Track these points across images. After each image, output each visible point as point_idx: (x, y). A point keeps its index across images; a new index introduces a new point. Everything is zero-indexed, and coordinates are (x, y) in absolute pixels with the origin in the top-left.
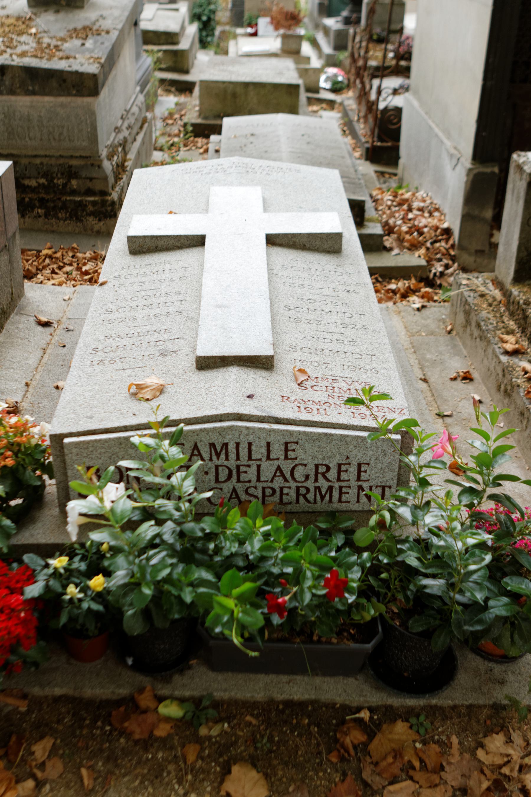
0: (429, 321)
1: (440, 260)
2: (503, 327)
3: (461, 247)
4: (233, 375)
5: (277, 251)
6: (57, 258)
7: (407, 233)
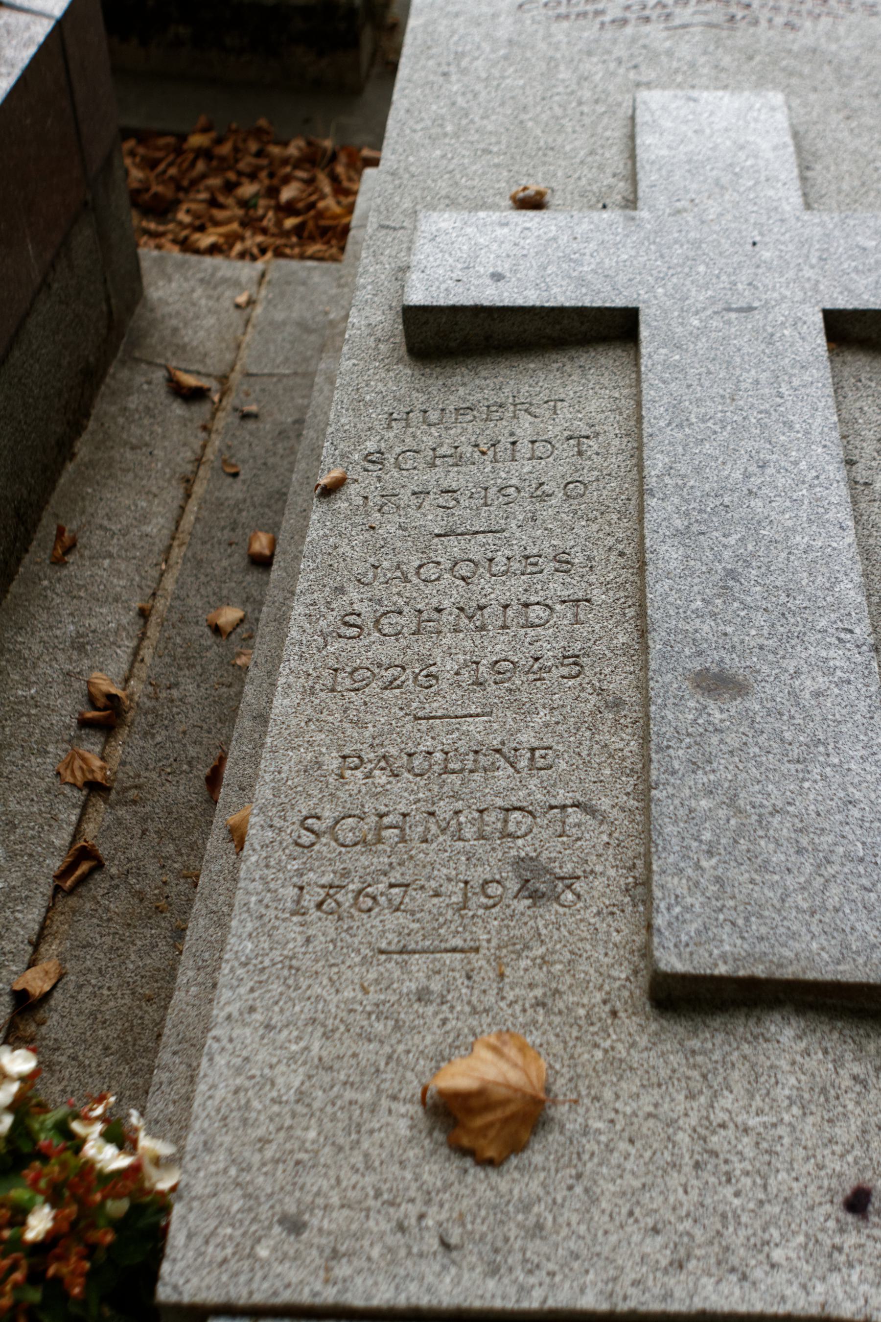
4: (784, 1065)
5: (859, 364)
6: (222, 159)
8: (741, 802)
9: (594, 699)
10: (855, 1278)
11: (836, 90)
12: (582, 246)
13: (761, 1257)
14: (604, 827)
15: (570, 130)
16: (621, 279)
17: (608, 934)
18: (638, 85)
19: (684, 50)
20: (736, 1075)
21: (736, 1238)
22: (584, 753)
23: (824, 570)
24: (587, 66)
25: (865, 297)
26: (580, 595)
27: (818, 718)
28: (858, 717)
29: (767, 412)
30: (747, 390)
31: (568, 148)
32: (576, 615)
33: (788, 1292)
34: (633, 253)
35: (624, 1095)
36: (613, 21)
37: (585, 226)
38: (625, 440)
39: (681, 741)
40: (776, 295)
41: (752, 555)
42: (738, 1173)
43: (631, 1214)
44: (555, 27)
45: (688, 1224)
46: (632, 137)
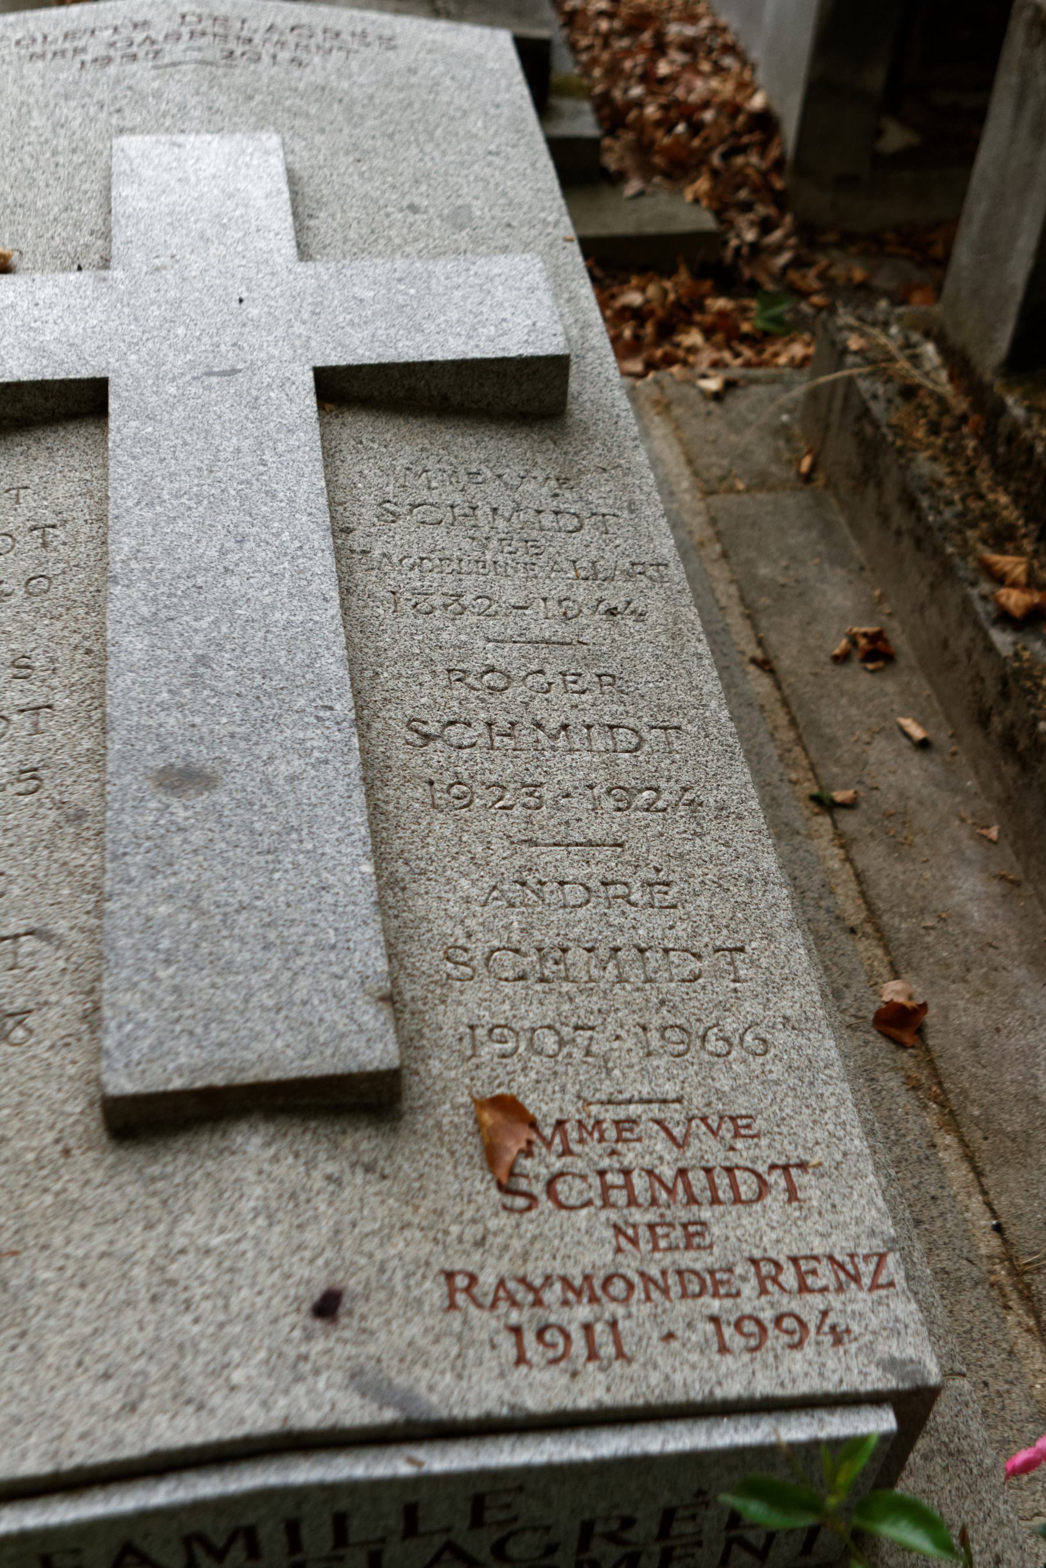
0: (749, 436)
1: (746, 207)
2: (984, 516)
3: (802, 165)
4: (250, 1175)
7: (658, 124)
8: (204, 904)
9: (53, 814)
10: (321, 1384)
11: (346, 131)
12: (44, 312)
13: (220, 1381)
14: (60, 953)
15: (42, 184)
16: (89, 347)
17: (62, 1067)
18: (121, 131)
19: (174, 91)
20: (198, 1195)
21: (193, 1367)
22: (41, 875)
23: (304, 646)
24: (65, 111)
25: (360, 351)
26: (41, 701)
27: (292, 804)
28: (335, 797)
29: (248, 482)
30: (226, 460)
31: (39, 204)
32: (36, 724)
33: (248, 1412)
34: (103, 318)
35: (76, 1238)
36: (95, 60)
37: (49, 291)
38: (95, 526)
39: (140, 846)
40: (262, 355)
41: (226, 637)
42: (197, 1298)
43: (80, 1364)
44: (27, 68)
45: (142, 1363)
46: (108, 189)
